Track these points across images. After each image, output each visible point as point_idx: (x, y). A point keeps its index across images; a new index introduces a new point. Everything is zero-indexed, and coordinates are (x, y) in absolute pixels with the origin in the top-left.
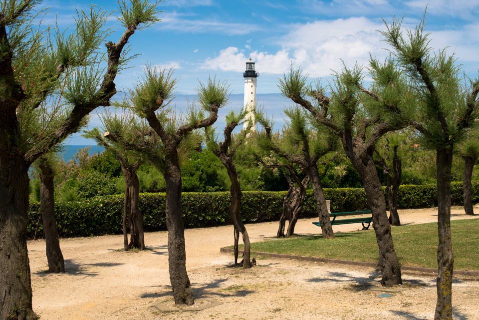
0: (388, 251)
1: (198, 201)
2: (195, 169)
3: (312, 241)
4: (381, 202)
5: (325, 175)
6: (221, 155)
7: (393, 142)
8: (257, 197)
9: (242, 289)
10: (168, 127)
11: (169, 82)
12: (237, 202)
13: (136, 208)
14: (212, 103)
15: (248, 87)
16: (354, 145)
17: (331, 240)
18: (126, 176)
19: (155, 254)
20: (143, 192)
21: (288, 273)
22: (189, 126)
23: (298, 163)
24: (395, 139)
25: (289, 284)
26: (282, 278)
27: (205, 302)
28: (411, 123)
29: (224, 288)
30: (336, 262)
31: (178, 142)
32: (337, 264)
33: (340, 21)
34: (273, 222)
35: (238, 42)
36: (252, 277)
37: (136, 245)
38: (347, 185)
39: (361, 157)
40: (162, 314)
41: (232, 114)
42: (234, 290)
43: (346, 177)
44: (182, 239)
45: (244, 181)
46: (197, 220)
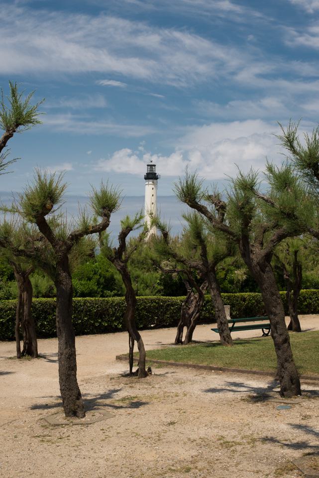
0: (286, 361)
1: (95, 307)
2: (92, 273)
3: (210, 348)
4: (279, 310)
5: (225, 279)
6: (115, 261)
7: (293, 247)
8: (155, 302)
9: (135, 400)
10: (59, 232)
11: (60, 186)
12: (131, 309)
13: (30, 313)
14: (104, 208)
15: (149, 188)
16: (252, 251)
17: (229, 348)
18: (19, 281)
19: (48, 361)
20: (38, 297)
21: (184, 383)
22: (80, 232)
23: (196, 268)
24: (295, 244)
25: (185, 395)
26: (178, 388)
27: (97, 414)
28: (309, 231)
29: (117, 399)
30: (234, 371)
31: (69, 249)
32: (235, 373)
33: (236, 123)
34: (171, 329)
35: (132, 144)
36: (146, 387)
37: (29, 352)
38: (248, 290)
39: (258, 264)
40: (51, 428)
41: (128, 218)
42: (127, 402)
43: (246, 281)
44: (73, 349)
45: (143, 285)
46: (93, 326)
